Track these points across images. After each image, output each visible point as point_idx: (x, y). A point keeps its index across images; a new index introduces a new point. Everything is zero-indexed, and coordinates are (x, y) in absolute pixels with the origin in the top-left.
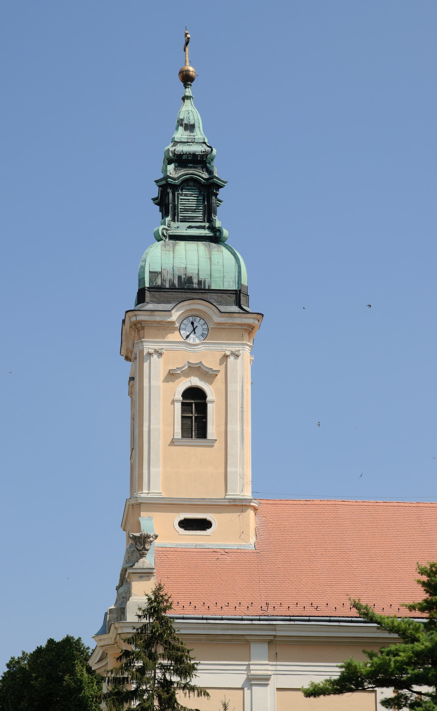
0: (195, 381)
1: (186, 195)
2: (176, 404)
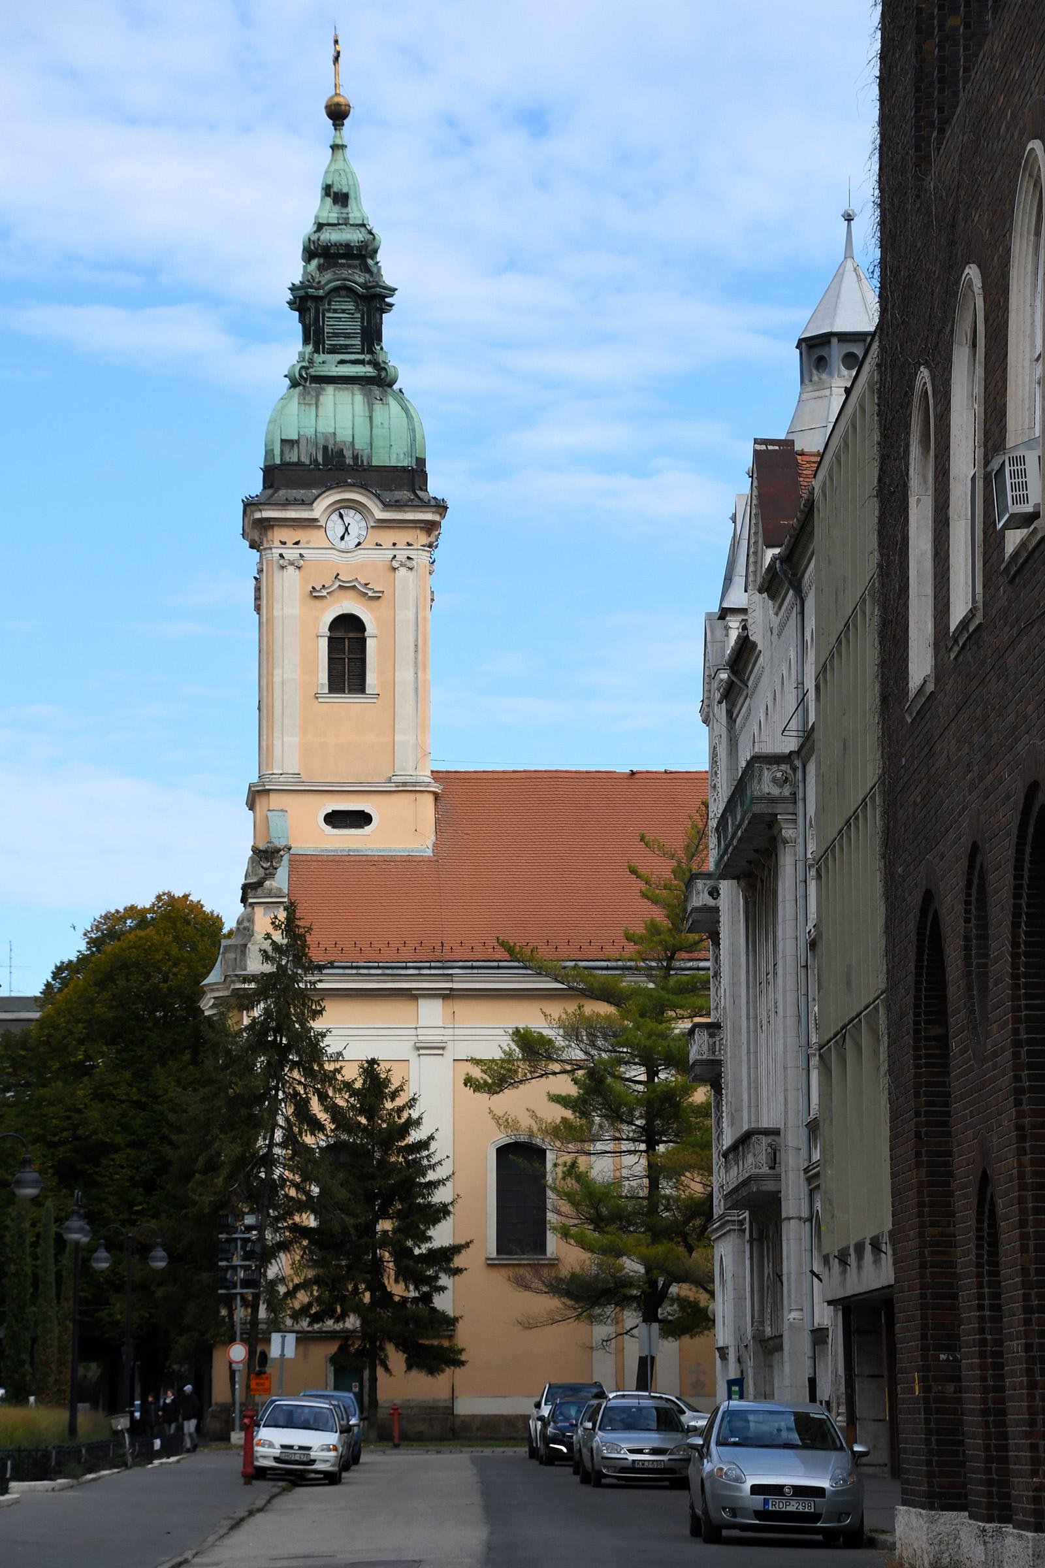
0: (349, 605)
1: (335, 311)
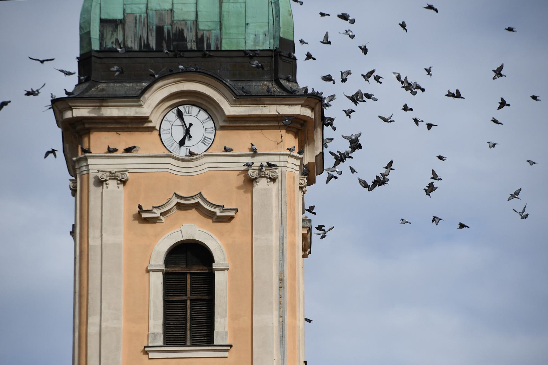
0: (193, 229)
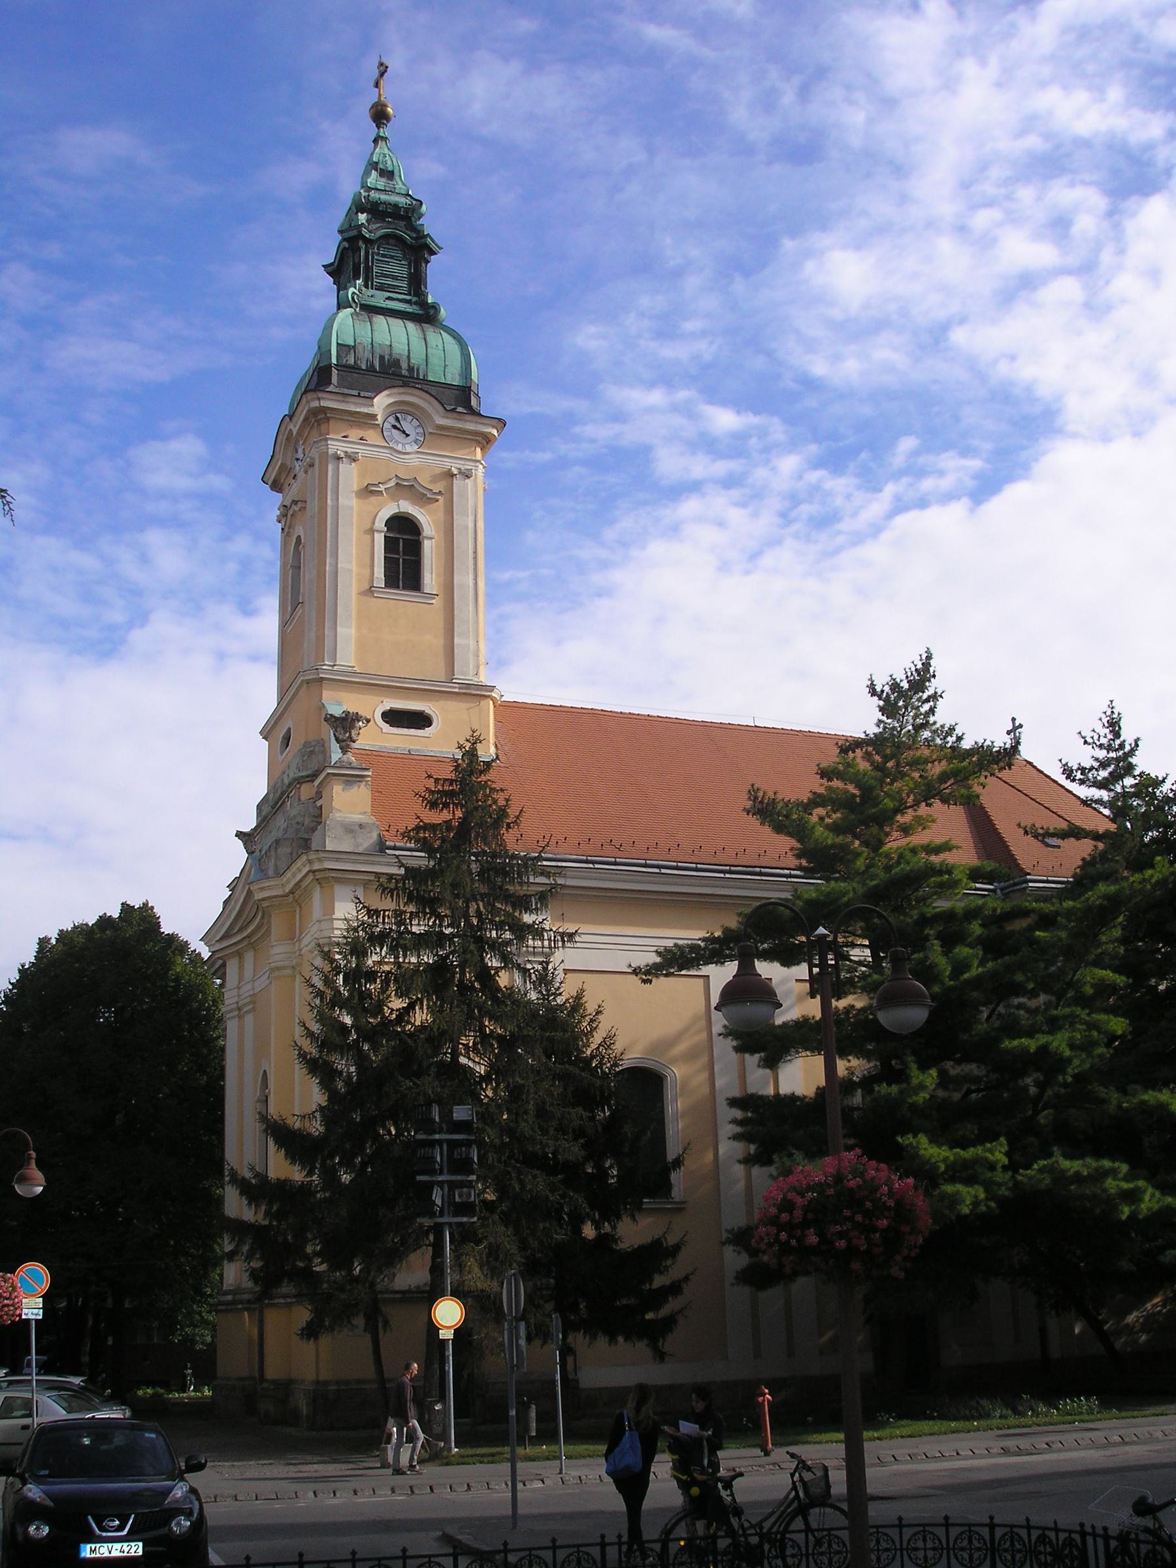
0: (407, 507)
1: (384, 256)
2: (376, 534)
